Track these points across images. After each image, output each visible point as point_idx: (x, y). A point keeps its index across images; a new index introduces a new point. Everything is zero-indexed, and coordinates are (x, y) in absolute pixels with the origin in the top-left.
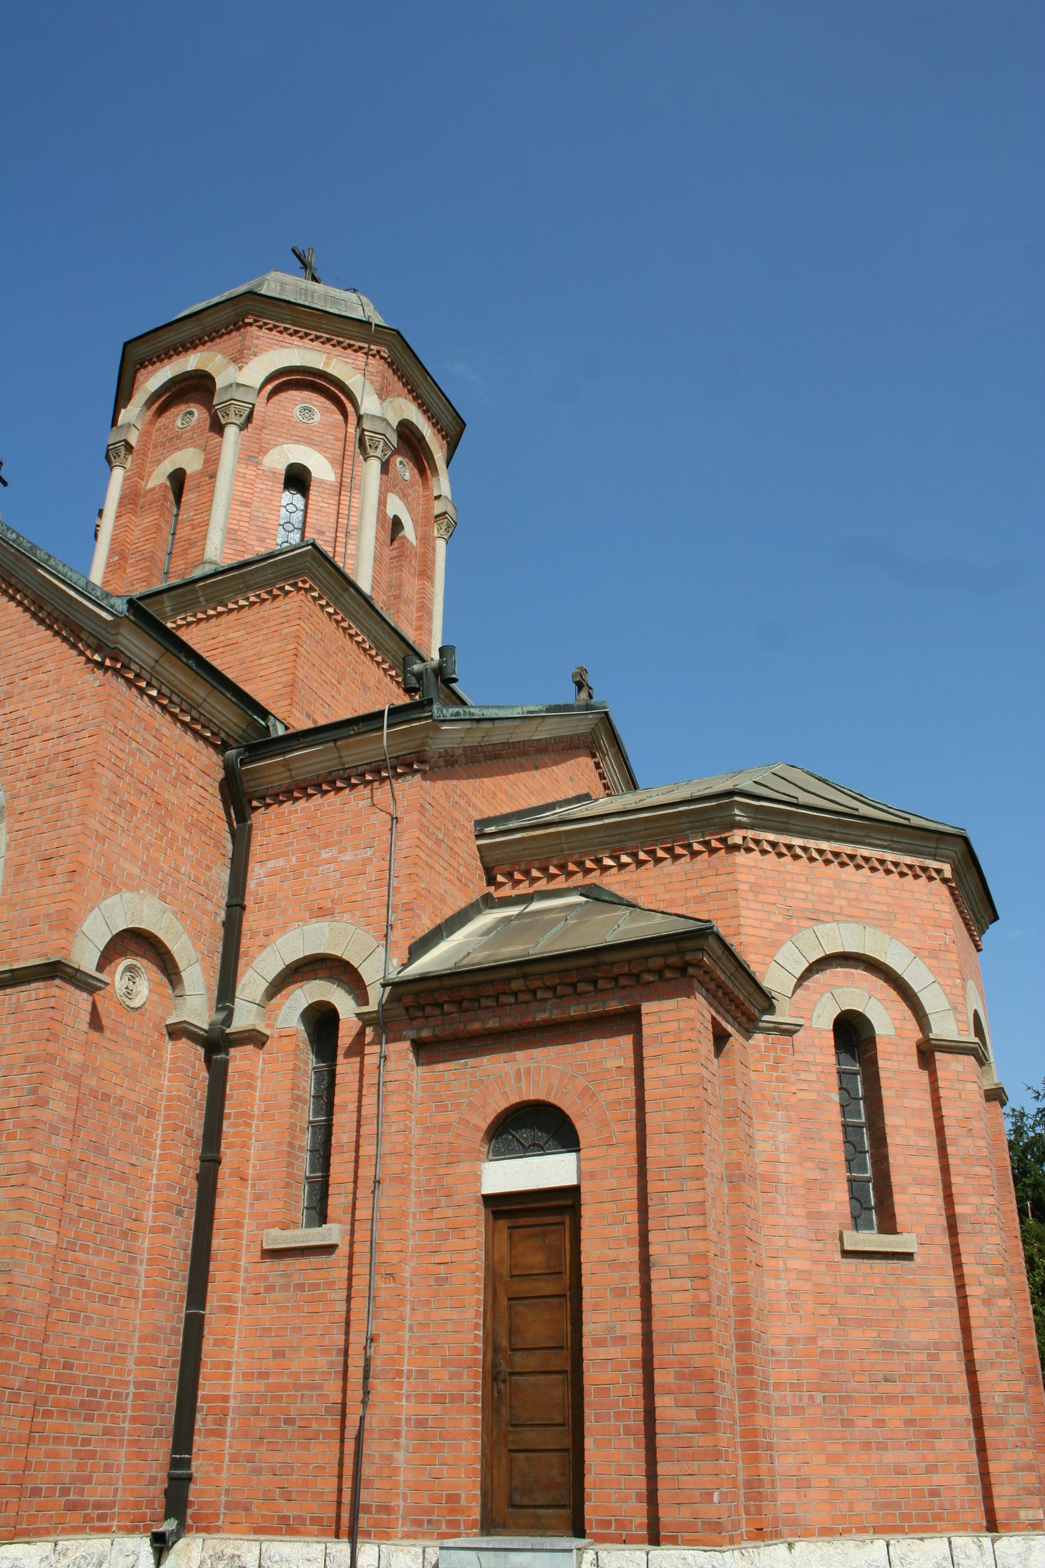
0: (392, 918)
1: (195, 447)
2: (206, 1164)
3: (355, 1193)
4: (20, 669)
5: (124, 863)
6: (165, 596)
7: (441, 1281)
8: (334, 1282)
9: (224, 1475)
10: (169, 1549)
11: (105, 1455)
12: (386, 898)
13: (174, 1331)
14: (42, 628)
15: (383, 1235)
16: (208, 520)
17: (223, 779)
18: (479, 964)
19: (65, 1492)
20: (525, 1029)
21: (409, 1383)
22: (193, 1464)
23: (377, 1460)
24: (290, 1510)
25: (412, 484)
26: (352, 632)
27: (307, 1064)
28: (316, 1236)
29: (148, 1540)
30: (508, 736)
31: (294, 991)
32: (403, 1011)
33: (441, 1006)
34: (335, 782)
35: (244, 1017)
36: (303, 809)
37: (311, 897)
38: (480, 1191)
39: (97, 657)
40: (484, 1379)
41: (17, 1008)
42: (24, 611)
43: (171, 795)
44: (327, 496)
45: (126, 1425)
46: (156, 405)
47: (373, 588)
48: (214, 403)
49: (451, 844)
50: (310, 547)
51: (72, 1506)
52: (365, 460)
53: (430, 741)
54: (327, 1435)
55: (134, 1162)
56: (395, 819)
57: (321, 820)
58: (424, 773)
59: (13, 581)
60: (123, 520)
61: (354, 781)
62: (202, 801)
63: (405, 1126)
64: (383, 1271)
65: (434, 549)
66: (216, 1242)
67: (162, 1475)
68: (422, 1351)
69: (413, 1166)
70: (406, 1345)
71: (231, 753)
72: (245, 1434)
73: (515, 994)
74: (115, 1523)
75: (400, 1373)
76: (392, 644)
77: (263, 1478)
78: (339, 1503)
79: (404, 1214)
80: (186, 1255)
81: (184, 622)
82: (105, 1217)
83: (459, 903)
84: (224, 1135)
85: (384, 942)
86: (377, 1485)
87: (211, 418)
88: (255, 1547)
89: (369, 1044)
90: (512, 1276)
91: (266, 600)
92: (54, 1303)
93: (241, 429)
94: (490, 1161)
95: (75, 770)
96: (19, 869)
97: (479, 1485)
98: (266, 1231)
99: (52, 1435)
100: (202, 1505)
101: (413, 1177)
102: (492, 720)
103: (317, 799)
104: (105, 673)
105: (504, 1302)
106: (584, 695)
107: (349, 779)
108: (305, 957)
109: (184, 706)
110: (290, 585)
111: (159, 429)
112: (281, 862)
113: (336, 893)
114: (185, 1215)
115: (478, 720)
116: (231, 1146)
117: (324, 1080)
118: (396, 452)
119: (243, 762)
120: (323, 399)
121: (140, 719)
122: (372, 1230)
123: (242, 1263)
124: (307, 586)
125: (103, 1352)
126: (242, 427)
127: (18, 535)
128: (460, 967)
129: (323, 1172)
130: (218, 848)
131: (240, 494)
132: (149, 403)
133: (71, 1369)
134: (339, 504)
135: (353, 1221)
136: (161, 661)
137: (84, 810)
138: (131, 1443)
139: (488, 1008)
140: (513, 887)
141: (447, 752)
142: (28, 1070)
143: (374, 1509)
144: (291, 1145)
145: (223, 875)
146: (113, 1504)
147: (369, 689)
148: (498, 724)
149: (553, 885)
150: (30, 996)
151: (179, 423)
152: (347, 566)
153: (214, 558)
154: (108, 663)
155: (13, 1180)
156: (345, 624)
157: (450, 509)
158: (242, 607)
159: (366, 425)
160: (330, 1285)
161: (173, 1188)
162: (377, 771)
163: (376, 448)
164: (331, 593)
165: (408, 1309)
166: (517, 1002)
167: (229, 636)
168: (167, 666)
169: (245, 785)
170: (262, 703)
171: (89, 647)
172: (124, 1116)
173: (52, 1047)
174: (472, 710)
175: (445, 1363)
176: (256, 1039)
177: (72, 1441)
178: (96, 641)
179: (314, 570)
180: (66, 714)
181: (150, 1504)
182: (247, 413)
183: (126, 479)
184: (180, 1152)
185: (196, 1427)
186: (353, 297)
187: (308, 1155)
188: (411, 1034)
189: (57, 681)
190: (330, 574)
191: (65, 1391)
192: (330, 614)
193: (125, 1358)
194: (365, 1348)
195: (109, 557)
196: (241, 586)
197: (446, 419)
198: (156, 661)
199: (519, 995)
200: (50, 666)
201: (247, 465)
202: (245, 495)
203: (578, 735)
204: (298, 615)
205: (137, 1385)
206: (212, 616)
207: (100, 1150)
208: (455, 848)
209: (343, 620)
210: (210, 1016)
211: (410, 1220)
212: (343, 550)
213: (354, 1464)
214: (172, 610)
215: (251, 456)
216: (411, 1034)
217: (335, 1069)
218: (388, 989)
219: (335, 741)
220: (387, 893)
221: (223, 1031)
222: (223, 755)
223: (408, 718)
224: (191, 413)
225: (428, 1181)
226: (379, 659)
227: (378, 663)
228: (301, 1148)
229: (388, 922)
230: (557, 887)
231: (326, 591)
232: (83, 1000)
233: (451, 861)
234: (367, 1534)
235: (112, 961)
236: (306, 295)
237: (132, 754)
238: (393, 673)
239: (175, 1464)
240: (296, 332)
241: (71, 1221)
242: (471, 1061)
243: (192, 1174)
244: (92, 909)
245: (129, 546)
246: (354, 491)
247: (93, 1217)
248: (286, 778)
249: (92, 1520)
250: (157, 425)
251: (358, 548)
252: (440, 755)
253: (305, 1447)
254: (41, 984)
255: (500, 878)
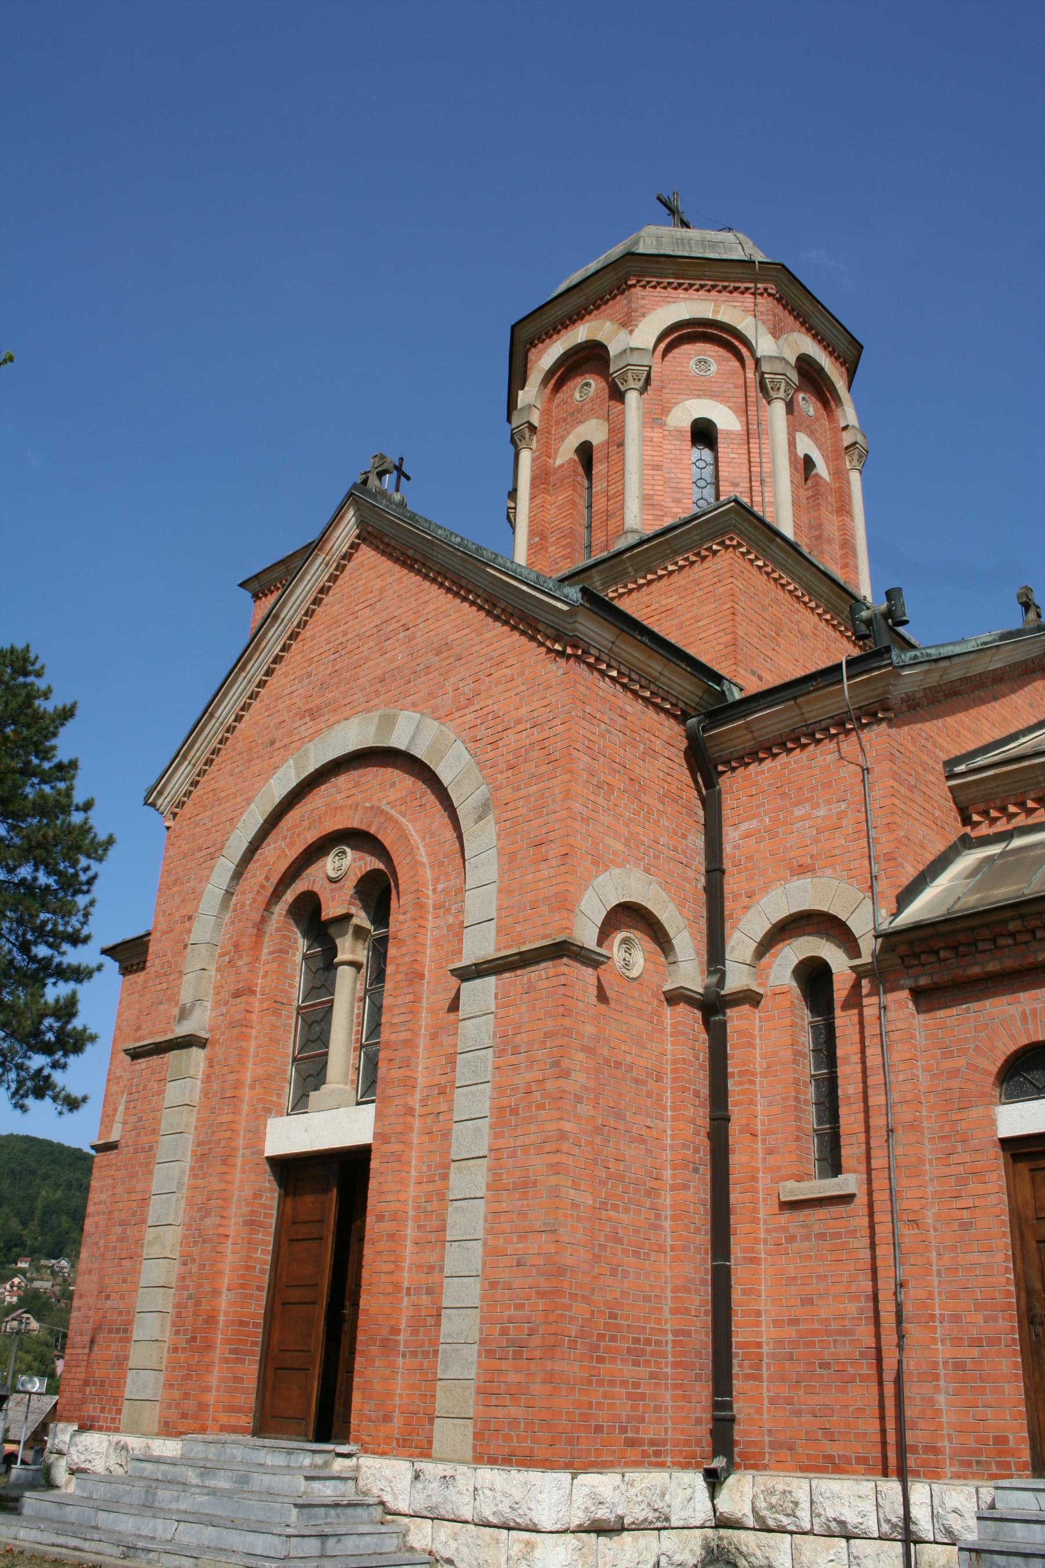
0: (875, 869)
1: (597, 418)
2: (715, 1122)
3: (868, 1143)
4: (483, 667)
5: (609, 841)
6: (593, 571)
7: (966, 1226)
8: (855, 1231)
9: (765, 1416)
10: (722, 1484)
11: (653, 1397)
12: (866, 850)
13: (703, 1281)
14: (498, 624)
15: (902, 1182)
16: (623, 489)
17: (686, 749)
18: (973, 908)
19: (623, 1430)
20: (1026, 970)
21: (942, 1327)
22: (735, 1406)
23: (918, 1402)
24: (834, 1450)
25: (817, 419)
26: (783, 581)
27: (803, 1019)
28: (831, 1186)
29: (701, 1475)
30: (964, 671)
31: (782, 950)
32: (899, 961)
33: (936, 953)
34: (799, 739)
35: (737, 979)
36: (769, 769)
37: (792, 855)
38: (996, 1135)
39: (557, 647)
40: (1020, 1322)
41: (528, 988)
42: (478, 610)
43: (641, 770)
44: (736, 446)
45: (669, 1370)
46: (553, 382)
47: (795, 533)
48: (611, 371)
49: (923, 788)
50: (732, 504)
51: (631, 1443)
52: (769, 403)
53: (892, 688)
54: (864, 1378)
55: (649, 1124)
56: (866, 770)
57: (789, 778)
58: (888, 720)
59: (463, 583)
60: (538, 501)
61: (818, 736)
62: (670, 771)
63: (912, 1074)
64: (905, 1218)
65: (848, 482)
66: (734, 1197)
67: (707, 1416)
68: (952, 1295)
69: (924, 1113)
70: (936, 1290)
71: (692, 721)
72: (783, 1379)
73: (1013, 935)
74: (669, 1459)
75: (932, 1317)
76: (823, 588)
77: (803, 1419)
78: (884, 1443)
79: (921, 1161)
80: (706, 1210)
81: (615, 594)
82: (630, 1178)
83: (939, 847)
84: (730, 1094)
85: (870, 894)
86: (921, 1424)
87: (609, 387)
88: (805, 1484)
89: (867, 996)
90: (1038, 1219)
91: (695, 562)
92: (596, 1258)
93: (641, 393)
94: (1004, 1104)
95: (553, 757)
96: (513, 857)
97: (1026, 1427)
98: (781, 1184)
99: (607, 1378)
100: (748, 1444)
101: (925, 1124)
102: (949, 658)
103: (783, 758)
104: (568, 660)
105: (1033, 1245)
106: (1032, 615)
107: (813, 735)
108: (791, 915)
109: (643, 682)
110: (717, 544)
111: (558, 405)
112: (754, 824)
113: (814, 849)
114: (701, 1171)
115: (936, 661)
116: (738, 1103)
117: (821, 1034)
118: (798, 389)
119: (704, 730)
120: (716, 348)
121: (604, 700)
122: (890, 1179)
123: (761, 1216)
124: (735, 543)
125: (641, 1303)
126: (642, 391)
127: (462, 539)
128: (954, 913)
129: (830, 1123)
130: (690, 816)
131: (650, 458)
132: (545, 381)
133: (616, 1319)
134: (749, 453)
135: (869, 1171)
136: (617, 643)
137: (567, 795)
138: (676, 1386)
139: (986, 951)
140: (991, 825)
141: (908, 697)
142: (549, 1045)
143: (920, 1449)
144: (797, 1099)
145: (699, 841)
146: (664, 1442)
147: (807, 637)
148: (955, 661)
149: (1032, 820)
150: (540, 975)
151: (577, 396)
152: (767, 514)
153: (635, 527)
154: (569, 651)
155: (548, 1147)
156: (775, 575)
157: (860, 439)
158: (671, 573)
159: (765, 367)
160: (852, 1234)
161: (687, 1147)
162: (841, 724)
163: (779, 389)
164: (758, 546)
165: (934, 1254)
166: (1016, 943)
167: (664, 602)
168: (623, 646)
169: (709, 751)
170: (708, 664)
171: (548, 637)
172: (636, 1081)
173: (567, 1022)
174: (929, 651)
175: (978, 1307)
176: (750, 998)
177: (624, 1384)
178: (553, 631)
179: (739, 526)
180: (536, 705)
181: (698, 1442)
182: (644, 376)
183: (533, 460)
184: (690, 1113)
185: (734, 1372)
186: (729, 236)
187: (813, 1109)
188: (910, 983)
189: (522, 673)
190: (755, 527)
191: (613, 1338)
192: (759, 567)
193: (661, 1309)
194: (895, 1294)
195: (530, 539)
196: (668, 551)
197: (843, 345)
198: (613, 643)
199: (1018, 936)
200: (512, 660)
201: (653, 428)
202: (655, 458)
203: (1032, 659)
204: (729, 574)
205: (675, 1333)
206: (642, 585)
207: (619, 1116)
208: (928, 791)
209: (773, 571)
210: (703, 980)
211: (927, 1167)
212: (760, 499)
213: (896, 1406)
214: (602, 584)
215: (655, 418)
216: (910, 983)
217: (833, 1023)
218: (880, 940)
219: (795, 698)
220: (866, 845)
221: (718, 993)
222: (684, 724)
223: (867, 668)
224: (588, 384)
225: (942, 1127)
226: (813, 604)
227: (812, 609)
228: (806, 1102)
229: (871, 873)
230: (1036, 821)
231: (753, 544)
232: (588, 974)
233: (926, 805)
234: (917, 1474)
235: (608, 936)
236: (683, 244)
237: (602, 735)
238: (828, 617)
239: (717, 1406)
240: (680, 285)
241: (601, 1182)
242: (973, 1006)
243: (703, 1132)
244: (586, 888)
245: (548, 526)
246: (763, 437)
247: (619, 1178)
248: (750, 740)
249: (648, 1456)
250: (556, 402)
251: (775, 495)
252: (903, 701)
253: (844, 1391)
254: (550, 964)
255: (976, 818)
